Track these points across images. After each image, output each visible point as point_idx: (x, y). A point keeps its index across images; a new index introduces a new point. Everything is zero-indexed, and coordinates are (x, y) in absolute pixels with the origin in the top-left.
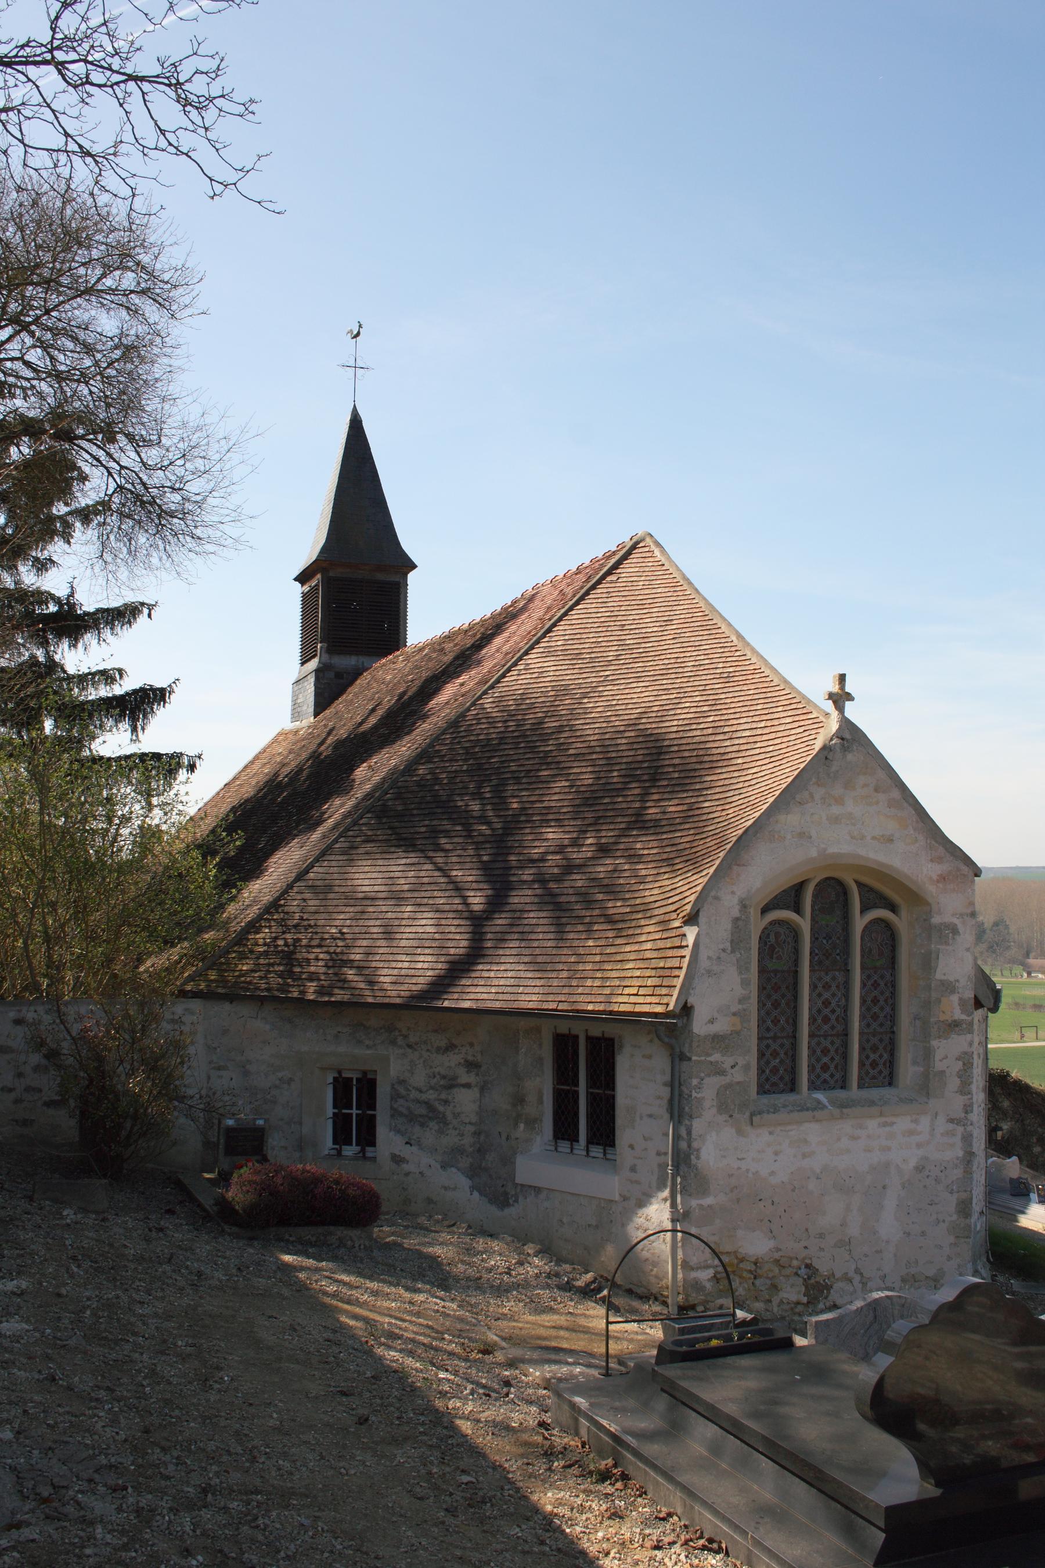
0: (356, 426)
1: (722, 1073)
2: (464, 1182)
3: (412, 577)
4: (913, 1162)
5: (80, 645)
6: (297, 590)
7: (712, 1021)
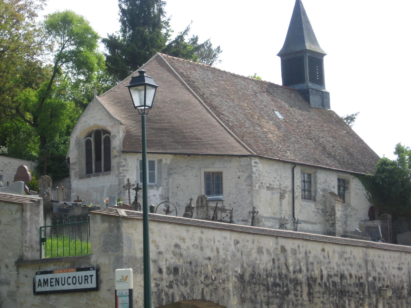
0: (299, 25)
1: (75, 169)
2: (23, 3)
3: (325, 58)
4: (109, 185)
5: (195, 36)
6: (279, 59)
7: (72, 160)
